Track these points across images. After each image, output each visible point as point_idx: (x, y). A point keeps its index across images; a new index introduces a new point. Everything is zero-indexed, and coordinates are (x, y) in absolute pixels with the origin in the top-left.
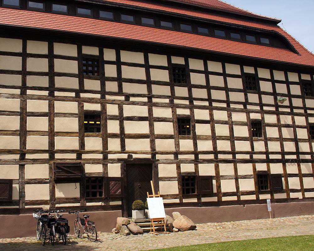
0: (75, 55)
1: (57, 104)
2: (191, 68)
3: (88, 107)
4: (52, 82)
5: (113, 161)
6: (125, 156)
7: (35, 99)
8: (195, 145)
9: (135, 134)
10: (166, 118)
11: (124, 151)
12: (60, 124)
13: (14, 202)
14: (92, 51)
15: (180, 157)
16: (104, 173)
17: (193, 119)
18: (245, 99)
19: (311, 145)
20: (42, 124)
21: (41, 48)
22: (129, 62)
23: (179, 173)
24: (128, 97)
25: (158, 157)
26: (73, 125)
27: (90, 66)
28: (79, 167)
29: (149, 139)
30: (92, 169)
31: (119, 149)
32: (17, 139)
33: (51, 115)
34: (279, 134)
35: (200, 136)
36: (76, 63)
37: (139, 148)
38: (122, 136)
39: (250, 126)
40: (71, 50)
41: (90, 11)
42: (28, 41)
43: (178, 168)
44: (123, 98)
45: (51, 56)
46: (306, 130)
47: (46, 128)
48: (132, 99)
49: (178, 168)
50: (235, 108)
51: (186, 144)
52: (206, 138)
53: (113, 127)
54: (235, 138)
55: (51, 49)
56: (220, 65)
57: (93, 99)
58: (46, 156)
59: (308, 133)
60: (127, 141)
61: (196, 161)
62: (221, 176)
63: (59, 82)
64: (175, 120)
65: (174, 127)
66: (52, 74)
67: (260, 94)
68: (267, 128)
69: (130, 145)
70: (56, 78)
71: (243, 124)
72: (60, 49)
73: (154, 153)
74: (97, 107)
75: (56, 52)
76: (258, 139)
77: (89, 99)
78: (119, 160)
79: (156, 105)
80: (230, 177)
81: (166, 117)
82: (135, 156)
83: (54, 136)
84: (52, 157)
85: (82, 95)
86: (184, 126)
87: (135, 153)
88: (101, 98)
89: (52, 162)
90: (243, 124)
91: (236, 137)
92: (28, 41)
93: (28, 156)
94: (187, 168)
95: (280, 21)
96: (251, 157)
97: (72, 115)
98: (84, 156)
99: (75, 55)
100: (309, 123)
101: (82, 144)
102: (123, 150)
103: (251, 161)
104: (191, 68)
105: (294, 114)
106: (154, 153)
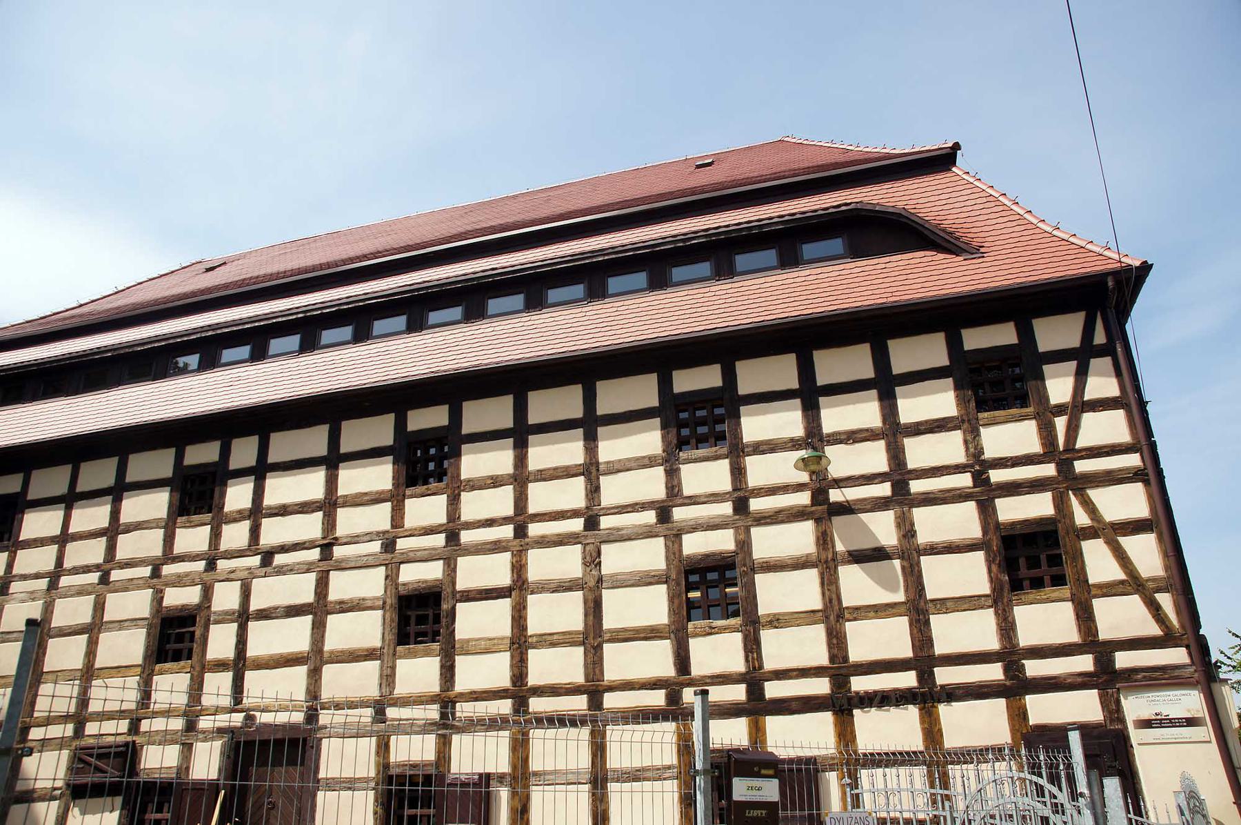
1: (922, 517)
2: (1042, 347)
3: (694, 545)
5: (209, 735)
6: (237, 719)
7: (72, 596)
9: (271, 656)
10: (364, 599)
11: (239, 707)
12: (942, 578)
14: (707, 378)
15: (391, 712)
16: (179, 769)
17: (449, 590)
18: (667, 488)
19: (1005, 619)
20: (566, 613)
21: (854, 362)
23: (384, 766)
24: (268, 556)
25: (325, 718)
26: (654, 606)
27: (703, 422)
28: (128, 754)
30: (158, 760)
31: (226, 701)
32: (577, 655)
34: (823, 594)
35: (468, 641)
37: (276, 695)
39: (678, 584)
41: (839, 241)
42: (892, 344)
43: (383, 748)
44: (255, 561)
46: (980, 556)
47: (814, 601)
48: (279, 559)
49: (383, 748)
50: (618, 529)
52: (487, 647)
53: (220, 642)
54: (607, 636)
57: (187, 574)
58: (579, 703)
62: (536, 774)
64: (389, 601)
65: (384, 623)
67: (738, 456)
71: (646, 579)
72: (908, 354)
73: (314, 704)
74: (724, 541)
76: (711, 628)
77: (179, 576)
79: (846, 509)
80: (570, 776)
81: (363, 596)
84: (79, 732)
85: (679, 514)
86: (420, 617)
87: (265, 710)
88: (206, 571)
89: (76, 743)
90: (646, 579)
91: (610, 631)
92: (892, 344)
94: (414, 750)
95: (957, 146)
99: (943, 360)
100: (997, 524)
103: (674, 711)
104: (1042, 347)
105: (913, 500)
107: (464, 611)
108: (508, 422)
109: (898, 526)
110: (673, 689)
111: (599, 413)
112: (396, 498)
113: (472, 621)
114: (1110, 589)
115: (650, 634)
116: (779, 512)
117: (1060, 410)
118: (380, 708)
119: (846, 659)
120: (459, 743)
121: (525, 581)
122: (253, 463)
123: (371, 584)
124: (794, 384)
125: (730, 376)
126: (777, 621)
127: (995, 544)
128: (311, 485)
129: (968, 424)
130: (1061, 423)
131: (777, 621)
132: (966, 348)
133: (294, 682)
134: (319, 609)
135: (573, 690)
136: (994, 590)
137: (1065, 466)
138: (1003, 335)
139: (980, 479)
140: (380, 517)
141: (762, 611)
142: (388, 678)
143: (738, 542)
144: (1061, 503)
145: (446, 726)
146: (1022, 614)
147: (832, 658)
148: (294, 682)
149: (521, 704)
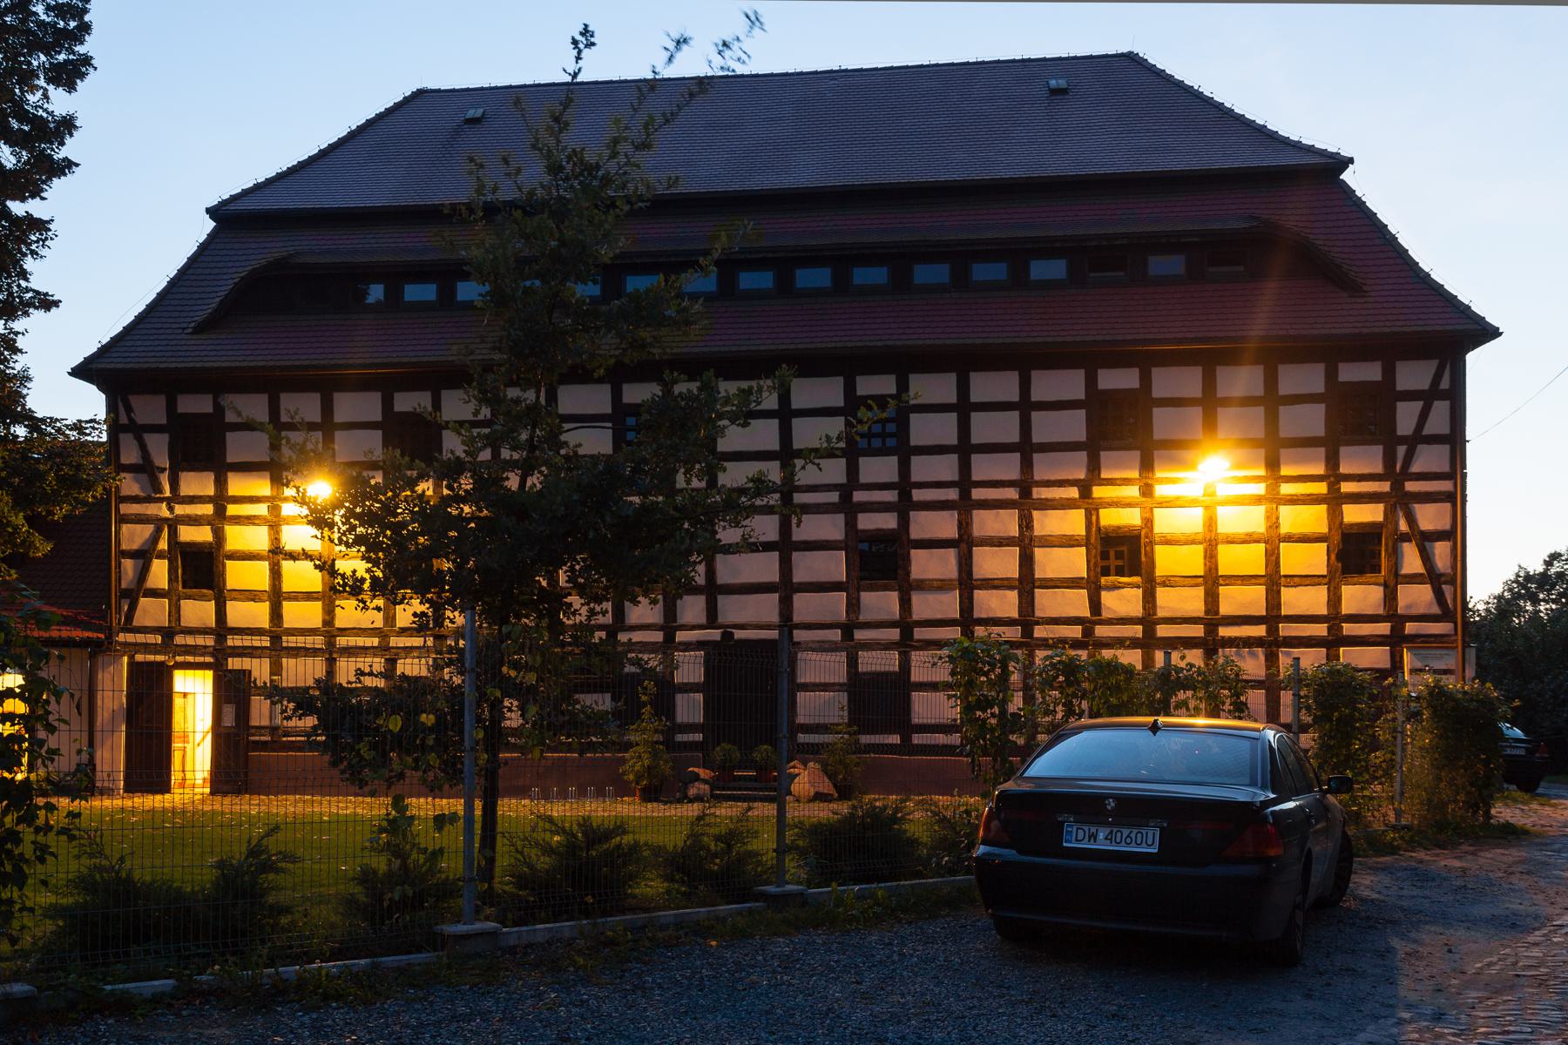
0: (1319, 386)
4: (965, 467)
5: (687, 646)
6: (715, 635)
8: (905, 604)
13: (1309, 726)
15: (860, 635)
22: (819, 405)
26: (835, 566)
29: (776, 595)
31: (703, 621)
32: (1013, 596)
33: (964, 544)
36: (1320, 409)
37: (752, 615)
38: (713, 590)
40: (829, 391)
45: (964, 408)
49: (852, 662)
51: (881, 603)
52: (942, 586)
55: (963, 388)
56: (160, 401)
59: (1333, 557)
60: (722, 600)
61: (1333, 642)
63: (983, 467)
66: (965, 449)
68: (230, 565)
69: (733, 610)
70: (915, 460)
73: (787, 622)
75: (797, 403)
78: (700, 645)
82: (739, 634)
83: (973, 588)
86: (881, 561)
92: (973, 375)
93: (894, 634)
96: (1088, 632)
97: (1168, 542)
98: (623, 637)
99: (1080, 394)
100: (857, 531)
101: (1095, 605)
102: (712, 620)
106: (787, 622)
107: (917, 555)
108: (951, 397)
109: (1268, 518)
110: (848, 629)
111: (1399, 388)
112: (852, 454)
113: (925, 564)
114: (1413, 579)
115: (1073, 583)
116: (818, 505)
117: (1403, 440)
118: (848, 629)
119: (1217, 613)
120: (917, 657)
121: (970, 535)
122: (1426, 387)
123: (830, 527)
124: (953, 399)
125: (1389, 373)
126: (1168, 582)
127: (1337, 538)
128: (765, 434)
129: (852, 454)
130: (1401, 450)
131: (1168, 582)
132: (1341, 379)
133: (766, 608)
134: (785, 547)
135: (1010, 622)
136: (1329, 572)
137: (1397, 486)
138: (1370, 372)
139: (965, 495)
140: (835, 471)
141: (1158, 572)
142: (853, 606)
143: (1143, 519)
144: (1390, 514)
145: (906, 644)
146: (867, 598)
147: (1207, 612)
148: (766, 608)
149: (330, 643)
